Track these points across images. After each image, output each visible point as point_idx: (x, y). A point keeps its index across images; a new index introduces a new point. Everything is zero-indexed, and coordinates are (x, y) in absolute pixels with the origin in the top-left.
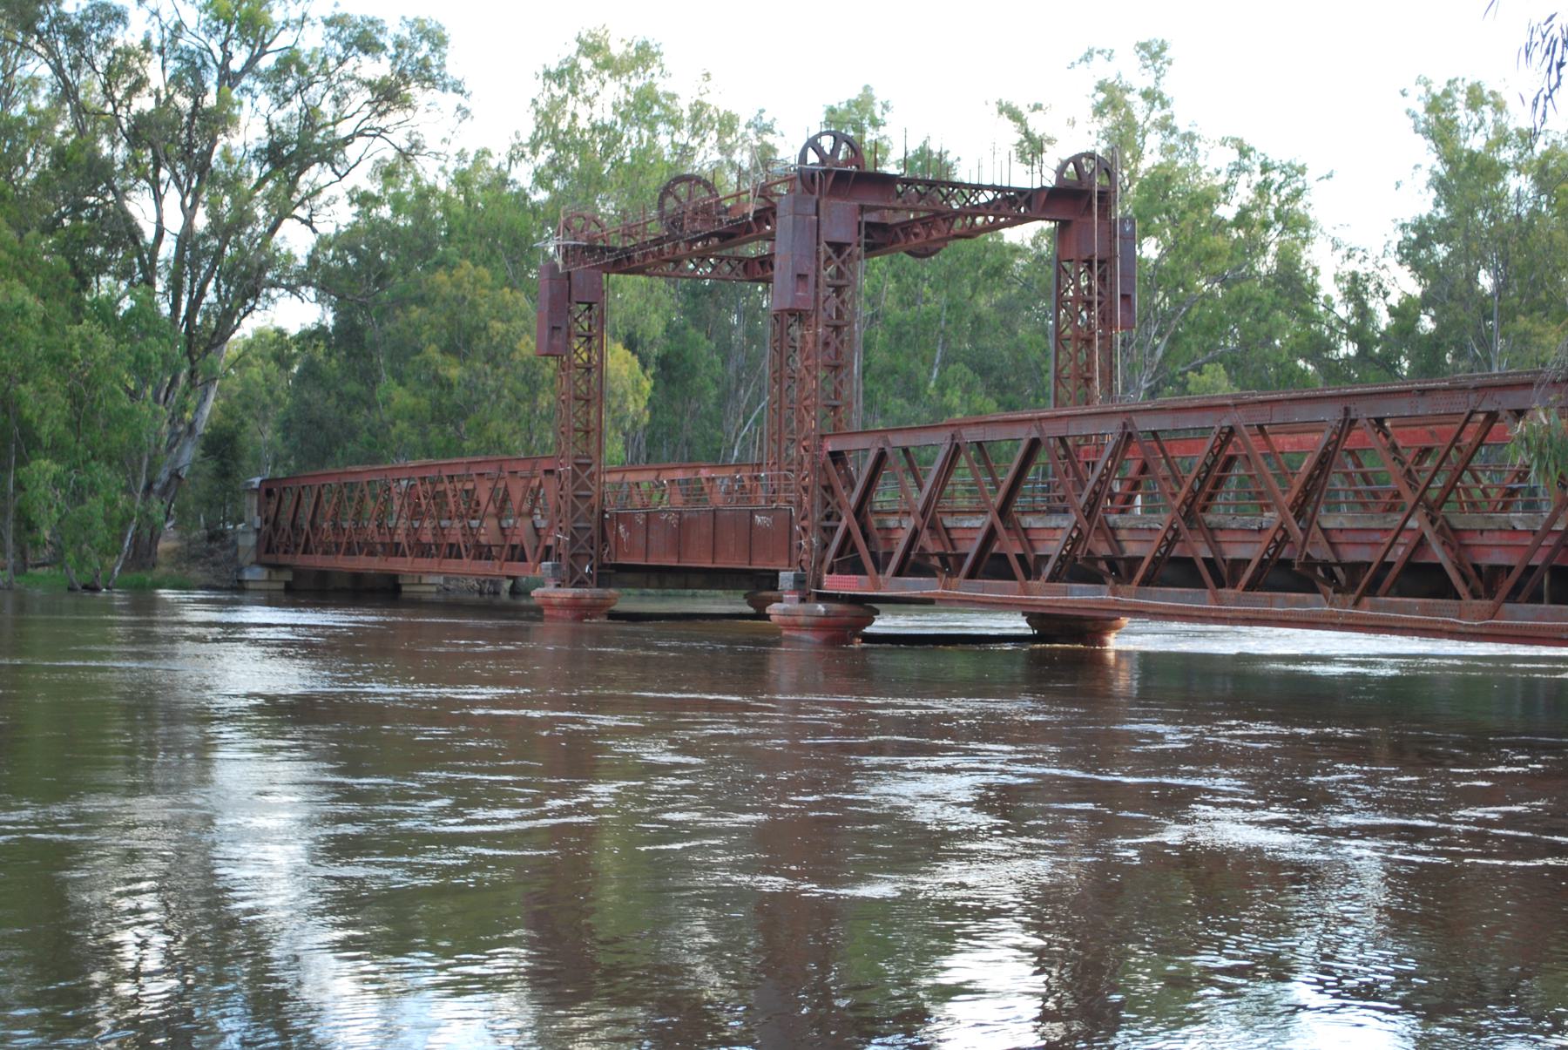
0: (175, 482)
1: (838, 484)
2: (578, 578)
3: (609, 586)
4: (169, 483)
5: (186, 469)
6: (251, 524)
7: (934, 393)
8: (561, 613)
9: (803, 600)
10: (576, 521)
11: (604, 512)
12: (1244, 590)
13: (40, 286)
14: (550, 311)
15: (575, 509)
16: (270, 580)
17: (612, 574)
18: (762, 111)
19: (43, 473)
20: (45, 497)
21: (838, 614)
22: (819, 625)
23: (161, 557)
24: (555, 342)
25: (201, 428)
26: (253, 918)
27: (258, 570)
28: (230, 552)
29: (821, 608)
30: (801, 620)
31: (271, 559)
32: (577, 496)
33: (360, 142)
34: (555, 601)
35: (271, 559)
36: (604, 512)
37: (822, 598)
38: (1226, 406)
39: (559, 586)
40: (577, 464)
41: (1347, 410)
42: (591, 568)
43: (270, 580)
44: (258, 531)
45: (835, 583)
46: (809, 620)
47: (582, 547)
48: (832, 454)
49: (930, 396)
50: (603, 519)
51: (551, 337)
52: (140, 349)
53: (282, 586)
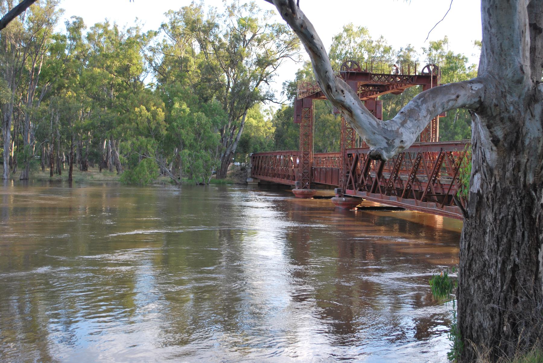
0: (231, 154)
1: (349, 165)
2: (304, 186)
3: (314, 188)
4: (230, 155)
5: (234, 151)
6: (250, 166)
7: (453, 128)
8: (299, 196)
9: (340, 197)
10: (304, 170)
11: (312, 168)
12: (422, 201)
13: (189, 102)
14: (297, 110)
15: (304, 166)
16: (254, 182)
17: (314, 185)
18: (410, 45)
19: (185, 153)
20: (186, 160)
21: (349, 201)
22: (344, 204)
23: (227, 175)
24: (298, 119)
25: (238, 139)
26: (378, 267)
27: (251, 179)
28: (246, 174)
29: (344, 199)
30: (338, 202)
31: (253, 176)
32: (304, 163)
33: (281, 59)
34: (297, 193)
35: (253, 176)
36: (312, 168)
37: (345, 196)
38: (418, 146)
39: (299, 188)
40: (304, 154)
41: (442, 149)
42: (308, 183)
43: (254, 182)
44: (251, 168)
45: (349, 192)
46: (340, 202)
47: (306, 177)
48: (348, 154)
49: (451, 129)
50: (312, 170)
51: (297, 118)
52: (215, 119)
53: (257, 184)
